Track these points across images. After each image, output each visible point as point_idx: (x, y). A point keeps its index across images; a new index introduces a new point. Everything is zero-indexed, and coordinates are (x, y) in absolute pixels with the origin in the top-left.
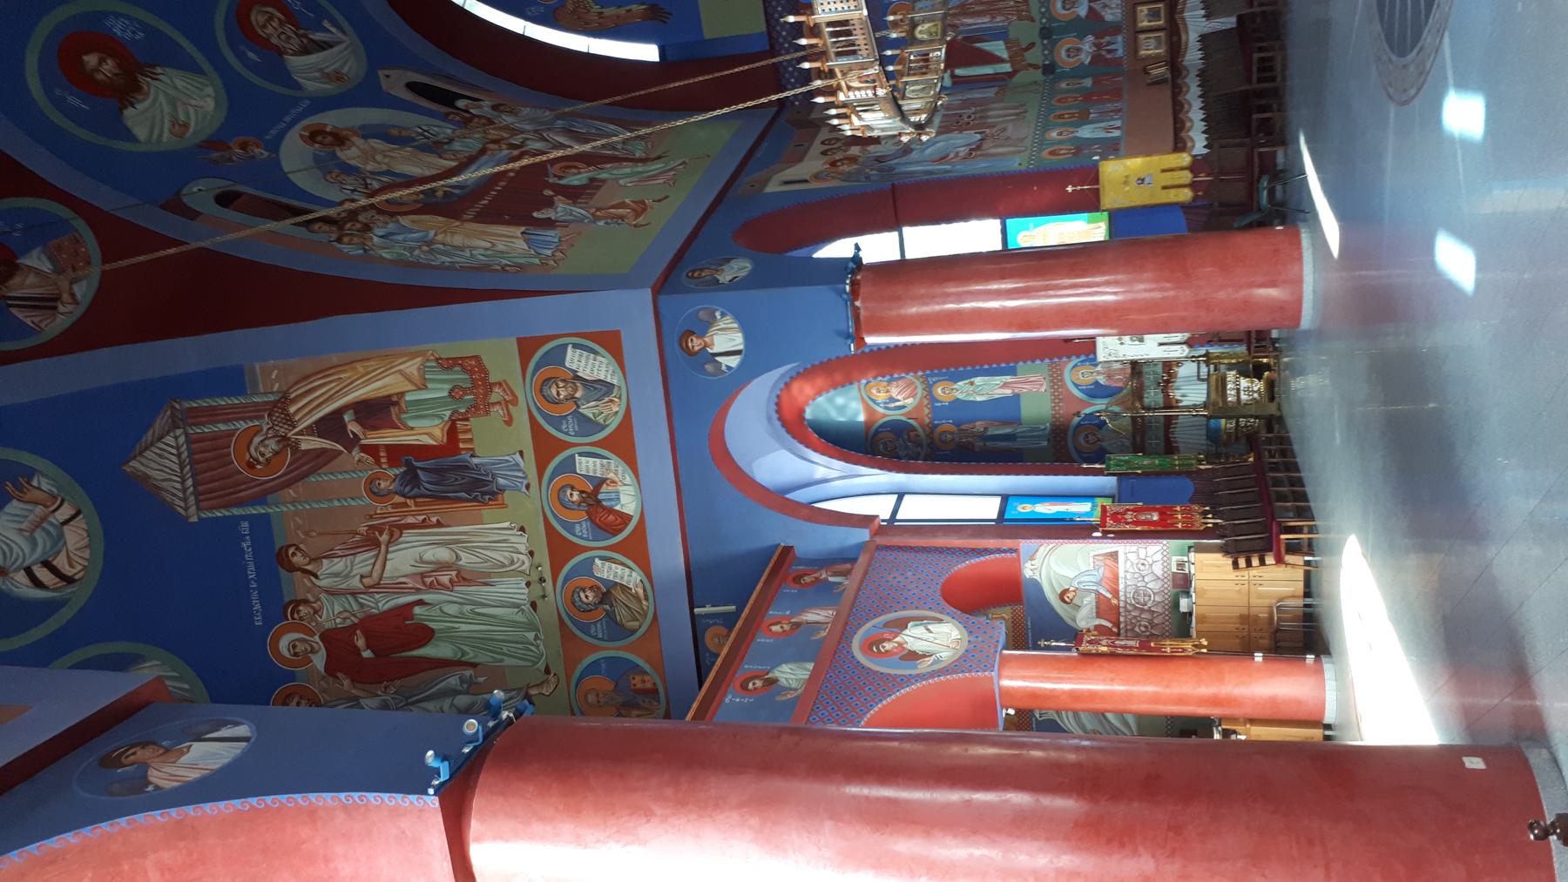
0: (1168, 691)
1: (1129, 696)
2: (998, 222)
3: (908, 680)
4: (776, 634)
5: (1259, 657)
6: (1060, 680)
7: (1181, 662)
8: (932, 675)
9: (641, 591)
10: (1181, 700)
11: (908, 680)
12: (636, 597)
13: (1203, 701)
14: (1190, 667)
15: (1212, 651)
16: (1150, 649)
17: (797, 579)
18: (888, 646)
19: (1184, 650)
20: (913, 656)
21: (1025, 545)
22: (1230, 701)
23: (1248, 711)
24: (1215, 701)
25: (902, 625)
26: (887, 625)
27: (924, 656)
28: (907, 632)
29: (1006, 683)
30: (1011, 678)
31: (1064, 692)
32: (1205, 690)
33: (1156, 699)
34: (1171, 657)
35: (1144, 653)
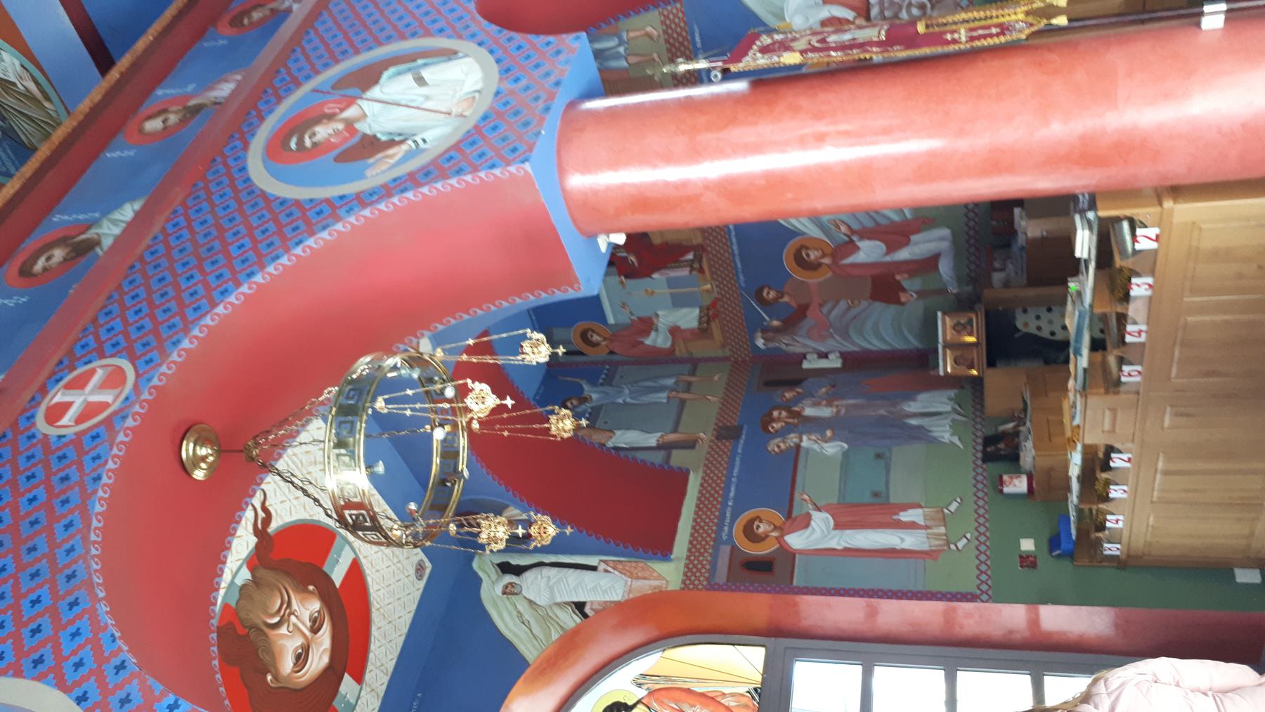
0: (963, 144)
1: (864, 172)
2: (856, 671)
3: (333, 209)
4: (154, 136)
5: (1213, 18)
6: (695, 154)
7: (995, 64)
8: (413, 180)
9: (32, 86)
10: (995, 163)
11: (333, 209)
12: (29, 96)
13: (1054, 159)
14: (1022, 75)
15: (1079, 22)
16: (912, 40)
17: (236, 22)
18: (323, 132)
19: (1004, 29)
20: (371, 146)
21: (925, 547)
22: (1128, 146)
23: (1176, 168)
24: (1086, 153)
25: (368, 78)
26: (340, 84)
27: (392, 143)
28: (375, 92)
29: (577, 181)
30: (586, 169)
31: (708, 186)
32: (1061, 129)
33: (928, 168)
34: (973, 55)
35: (901, 53)
